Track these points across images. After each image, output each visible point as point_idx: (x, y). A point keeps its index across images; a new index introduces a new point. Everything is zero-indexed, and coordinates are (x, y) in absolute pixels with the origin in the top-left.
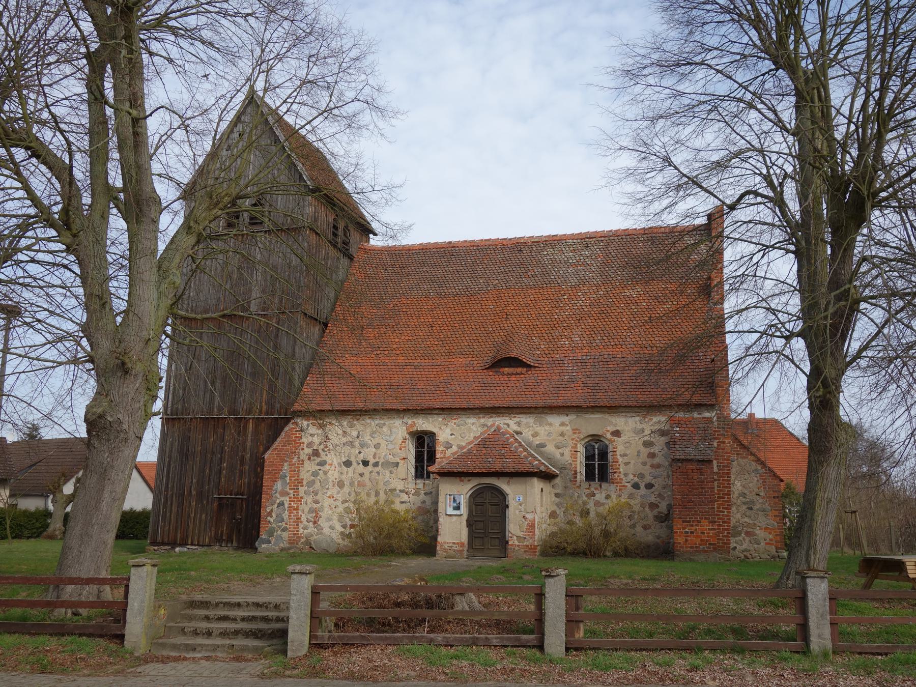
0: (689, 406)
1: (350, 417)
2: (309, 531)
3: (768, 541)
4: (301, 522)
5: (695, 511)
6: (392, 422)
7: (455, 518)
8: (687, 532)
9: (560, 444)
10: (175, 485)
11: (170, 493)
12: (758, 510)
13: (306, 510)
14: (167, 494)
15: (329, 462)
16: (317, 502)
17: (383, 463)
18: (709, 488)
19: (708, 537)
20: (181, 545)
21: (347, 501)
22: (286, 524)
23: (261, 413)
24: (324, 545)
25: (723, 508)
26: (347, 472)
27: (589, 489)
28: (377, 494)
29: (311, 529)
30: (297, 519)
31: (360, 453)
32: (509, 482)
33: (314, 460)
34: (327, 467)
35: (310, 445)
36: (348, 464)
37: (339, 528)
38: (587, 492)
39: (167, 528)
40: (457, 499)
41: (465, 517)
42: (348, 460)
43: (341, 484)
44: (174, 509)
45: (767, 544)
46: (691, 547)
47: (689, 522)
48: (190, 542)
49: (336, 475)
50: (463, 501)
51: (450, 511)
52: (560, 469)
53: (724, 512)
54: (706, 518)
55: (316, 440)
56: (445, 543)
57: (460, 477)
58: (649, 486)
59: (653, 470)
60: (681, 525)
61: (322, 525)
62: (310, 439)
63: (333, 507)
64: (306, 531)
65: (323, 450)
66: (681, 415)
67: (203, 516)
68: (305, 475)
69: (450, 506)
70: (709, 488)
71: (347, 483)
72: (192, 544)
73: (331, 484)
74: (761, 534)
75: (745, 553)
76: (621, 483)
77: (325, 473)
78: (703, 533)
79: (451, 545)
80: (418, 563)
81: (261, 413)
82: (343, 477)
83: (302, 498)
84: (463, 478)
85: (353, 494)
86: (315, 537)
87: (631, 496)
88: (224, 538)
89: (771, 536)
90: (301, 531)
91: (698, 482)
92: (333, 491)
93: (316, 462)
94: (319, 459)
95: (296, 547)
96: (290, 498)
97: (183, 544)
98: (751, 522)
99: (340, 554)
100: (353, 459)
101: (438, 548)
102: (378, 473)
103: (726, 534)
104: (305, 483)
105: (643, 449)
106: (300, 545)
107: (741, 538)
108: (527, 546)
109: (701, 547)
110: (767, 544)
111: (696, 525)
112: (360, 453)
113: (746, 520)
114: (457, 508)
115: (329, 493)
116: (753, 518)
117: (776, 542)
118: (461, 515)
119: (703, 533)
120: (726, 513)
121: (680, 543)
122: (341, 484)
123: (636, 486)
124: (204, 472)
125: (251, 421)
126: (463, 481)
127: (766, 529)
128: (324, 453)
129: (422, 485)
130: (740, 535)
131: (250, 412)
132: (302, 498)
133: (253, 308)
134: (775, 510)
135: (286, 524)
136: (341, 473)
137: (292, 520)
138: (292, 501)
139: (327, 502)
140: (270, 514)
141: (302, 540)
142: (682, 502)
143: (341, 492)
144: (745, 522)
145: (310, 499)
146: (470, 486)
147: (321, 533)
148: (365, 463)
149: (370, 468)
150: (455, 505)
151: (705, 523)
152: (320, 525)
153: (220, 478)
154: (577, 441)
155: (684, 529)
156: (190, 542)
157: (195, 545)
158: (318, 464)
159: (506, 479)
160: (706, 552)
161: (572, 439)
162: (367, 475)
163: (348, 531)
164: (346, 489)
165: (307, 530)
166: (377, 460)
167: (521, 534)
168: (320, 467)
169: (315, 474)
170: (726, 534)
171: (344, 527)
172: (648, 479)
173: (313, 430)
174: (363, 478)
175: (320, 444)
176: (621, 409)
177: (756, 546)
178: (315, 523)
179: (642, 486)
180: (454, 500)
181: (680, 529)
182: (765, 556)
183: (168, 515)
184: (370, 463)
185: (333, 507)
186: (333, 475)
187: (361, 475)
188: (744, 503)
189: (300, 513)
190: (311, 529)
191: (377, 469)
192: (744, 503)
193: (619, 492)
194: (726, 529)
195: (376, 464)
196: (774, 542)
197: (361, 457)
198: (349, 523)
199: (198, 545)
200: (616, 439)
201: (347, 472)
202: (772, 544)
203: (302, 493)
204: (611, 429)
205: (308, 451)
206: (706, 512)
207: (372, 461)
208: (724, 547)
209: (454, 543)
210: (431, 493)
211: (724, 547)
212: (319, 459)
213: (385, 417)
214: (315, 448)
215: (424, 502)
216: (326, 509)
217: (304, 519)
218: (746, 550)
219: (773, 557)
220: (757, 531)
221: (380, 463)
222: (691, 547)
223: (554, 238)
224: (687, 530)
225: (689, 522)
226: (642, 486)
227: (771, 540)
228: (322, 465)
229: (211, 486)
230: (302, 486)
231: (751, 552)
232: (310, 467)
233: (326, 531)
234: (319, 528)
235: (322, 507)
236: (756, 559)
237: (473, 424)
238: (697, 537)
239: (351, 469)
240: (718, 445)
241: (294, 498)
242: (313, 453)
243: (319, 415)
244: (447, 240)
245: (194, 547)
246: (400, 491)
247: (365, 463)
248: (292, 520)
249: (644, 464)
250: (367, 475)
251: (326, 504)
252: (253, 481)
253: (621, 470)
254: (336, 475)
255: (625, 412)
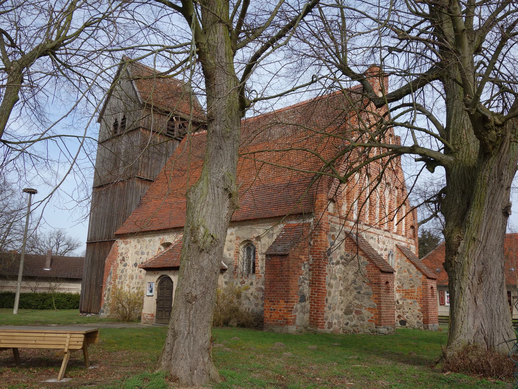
0: (299, 215)
3: (370, 318)
5: (277, 294)
6: (154, 238)
8: (271, 310)
9: (229, 248)
12: (364, 293)
18: (286, 276)
19: (283, 313)
25: (315, 292)
27: (241, 278)
31: (141, 258)
32: (174, 274)
38: (241, 280)
41: (155, 297)
45: (369, 321)
46: (274, 321)
47: (273, 302)
50: (155, 286)
51: (149, 293)
52: (229, 265)
53: (315, 295)
54: (283, 299)
57: (154, 271)
60: (268, 304)
66: (294, 222)
68: (119, 273)
70: (286, 276)
73: (128, 277)
74: (366, 313)
75: (354, 328)
76: (259, 274)
77: (126, 271)
78: (280, 310)
79: (147, 315)
84: (155, 272)
89: (372, 315)
91: (280, 271)
97: (90, 313)
98: (359, 303)
103: (315, 312)
107: (352, 316)
109: (279, 321)
110: (369, 321)
111: (277, 304)
113: (356, 301)
116: (360, 299)
117: (376, 319)
118: (152, 296)
119: (280, 310)
120: (316, 296)
121: (267, 318)
127: (369, 309)
130: (352, 313)
134: (376, 294)
140: (105, 296)
142: (270, 286)
144: (356, 303)
146: (158, 277)
151: (282, 302)
154: (238, 245)
155: (270, 307)
159: (172, 272)
160: (281, 325)
161: (236, 244)
170: (315, 312)
173: (123, 245)
177: (362, 322)
181: (267, 307)
182: (367, 331)
188: (355, 289)
192: (355, 289)
194: (316, 308)
196: (374, 319)
202: (373, 321)
204: (256, 235)
206: (283, 294)
208: (314, 322)
209: (148, 314)
211: (314, 322)
213: (152, 235)
218: (355, 326)
219: (373, 332)
220: (363, 311)
222: (274, 321)
223: (281, 110)
224: (271, 308)
225: (273, 302)
227: (372, 318)
228: (125, 266)
231: (358, 327)
232: (121, 267)
236: (360, 333)
238: (277, 313)
240: (314, 243)
253: (259, 264)
255: (263, 223)
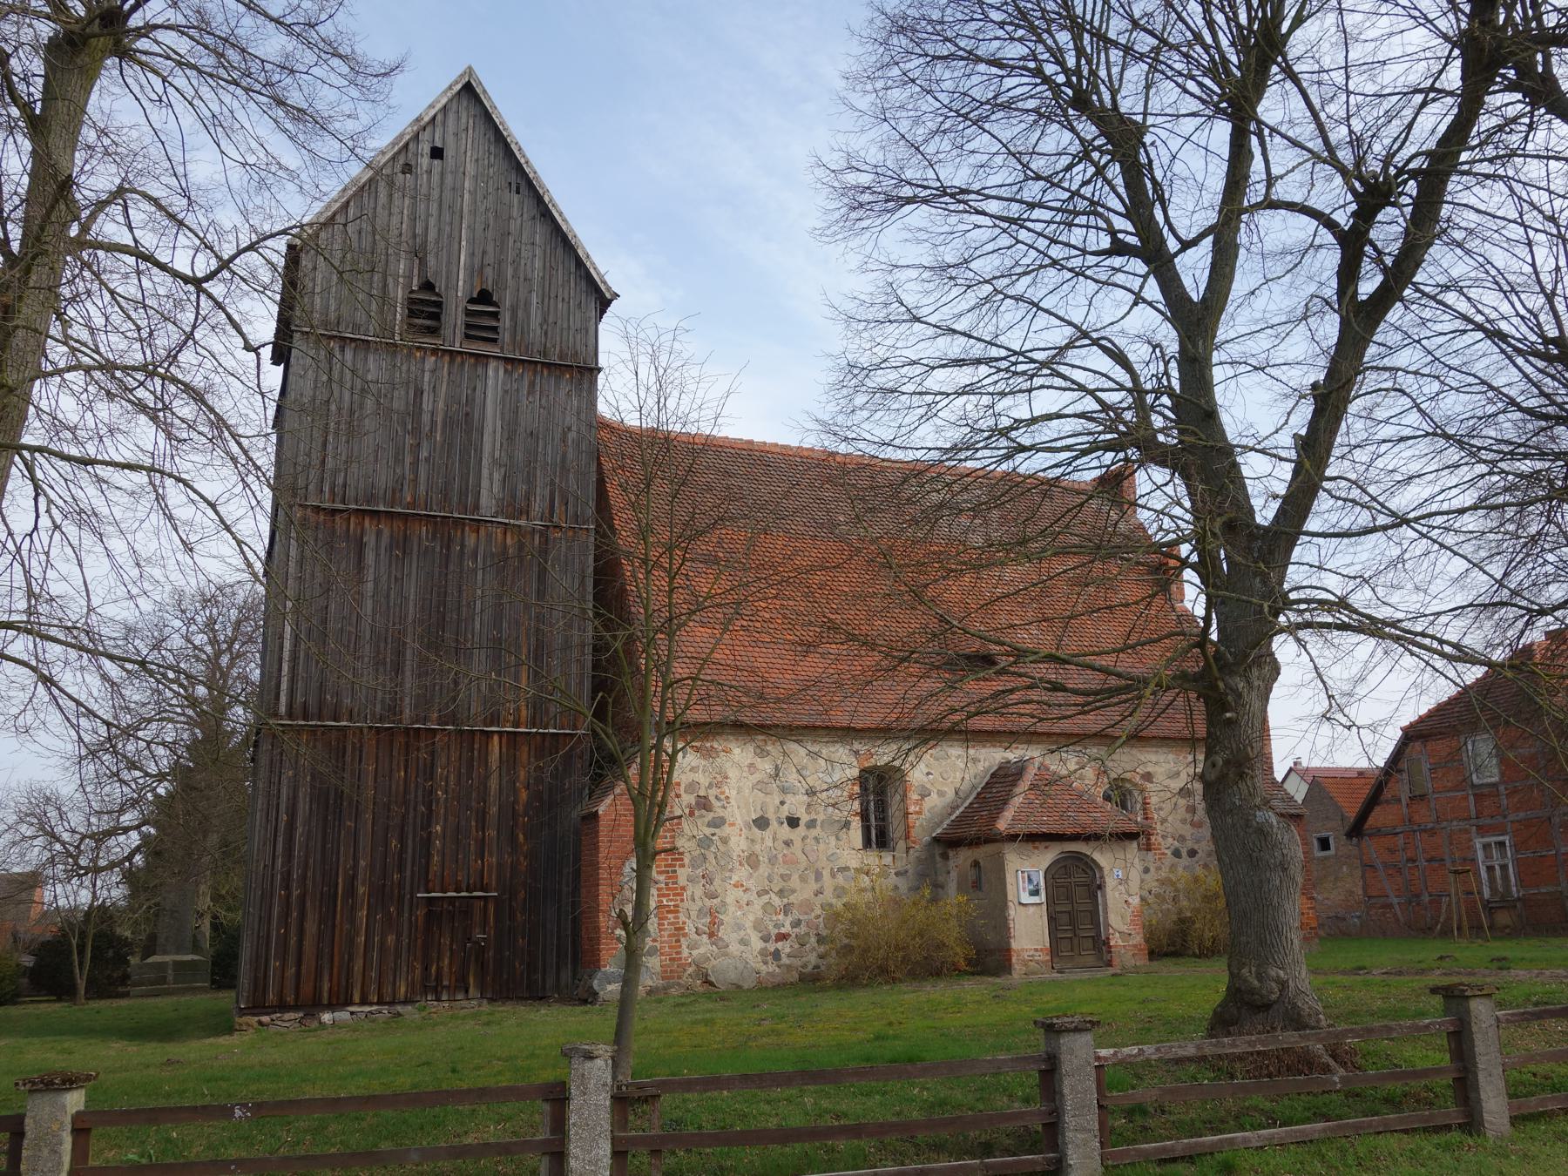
1: (760, 737)
2: (702, 950)
4: (685, 935)
6: (832, 749)
7: (1032, 909)
10: (310, 874)
11: (296, 893)
13: (694, 908)
14: (288, 896)
15: (730, 819)
16: (713, 896)
17: (823, 822)
20: (331, 1007)
21: (767, 892)
22: (654, 940)
23: (290, 715)
24: (732, 976)
26: (762, 839)
28: (819, 876)
29: (705, 947)
30: (676, 929)
31: (782, 803)
33: (702, 816)
34: (726, 830)
35: (692, 787)
36: (762, 823)
37: (757, 944)
39: (291, 971)
40: (1034, 878)
42: (762, 817)
43: (752, 861)
44: (311, 927)
48: (357, 998)
49: (744, 844)
51: (1026, 898)
55: (703, 779)
56: (1023, 950)
58: (1192, 853)
59: (1195, 831)
61: (725, 937)
62: (692, 776)
63: (743, 903)
64: (695, 953)
65: (717, 797)
67: (391, 939)
69: (1024, 889)
71: (763, 859)
72: (364, 1002)
77: (725, 841)
80: (973, 989)
81: (517, 724)
82: (757, 848)
83: (683, 888)
84: (1037, 844)
85: (776, 879)
86: (714, 962)
87: (1173, 867)
88: (446, 983)
90: (685, 952)
92: (741, 874)
93: (706, 820)
94: (710, 816)
95: (679, 984)
96: (659, 889)
99: (768, 989)
100: (771, 815)
101: (1014, 960)
102: (817, 839)
104: (686, 861)
105: (721, 813)
106: (685, 980)
108: (1135, 946)
112: (782, 803)
114: (1035, 893)
115: (735, 878)
122: (752, 861)
123: (1177, 854)
124: (386, 844)
125: (496, 738)
126: (1037, 848)
128: (718, 804)
129: (890, 859)
131: (494, 719)
132: (683, 888)
133: (487, 504)
135: (654, 940)
136: (753, 841)
137: (666, 934)
138: (664, 896)
139: (732, 896)
141: (690, 970)
143: (755, 875)
145: (698, 891)
147: (726, 955)
148: (793, 822)
149: (801, 830)
150: (1031, 887)
152: (721, 939)
153: (429, 856)
156: (357, 998)
157: (371, 1004)
158: (709, 825)
162: (798, 844)
163: (771, 947)
164: (764, 870)
165: (698, 949)
166: (813, 816)
167: (1124, 928)
168: (713, 830)
169: (705, 843)
171: (766, 939)
172: (1190, 844)
174: (792, 849)
175: (710, 786)
176: (1154, 741)
178: (711, 935)
179: (1184, 854)
180: (1030, 880)
183: (293, 941)
184: (802, 823)
185: (743, 903)
186: (738, 843)
187: (788, 843)
189: (682, 918)
190: (705, 947)
191: (814, 832)
193: (1159, 863)
195: (811, 824)
197: (785, 812)
198: (774, 932)
199: (378, 1003)
200: (1149, 785)
201: (762, 839)
203: (682, 881)
205: (688, 799)
207: (804, 818)
209: (1036, 950)
210: (906, 872)
212: (710, 816)
214: (702, 793)
215: (896, 888)
216: (731, 909)
217: (690, 928)
221: (819, 822)
226: (1184, 854)
229: (408, 873)
230: (683, 866)
233: (735, 948)
234: (720, 943)
235: (724, 903)
237: (959, 757)
239: (768, 833)
241: (668, 889)
242: (697, 804)
243: (702, 731)
244: (746, 438)
245: (367, 1009)
246: (857, 870)
247: (793, 822)
248: (666, 934)
249: (1184, 821)
250: (798, 844)
251: (730, 900)
252: (508, 859)
254: (744, 844)
